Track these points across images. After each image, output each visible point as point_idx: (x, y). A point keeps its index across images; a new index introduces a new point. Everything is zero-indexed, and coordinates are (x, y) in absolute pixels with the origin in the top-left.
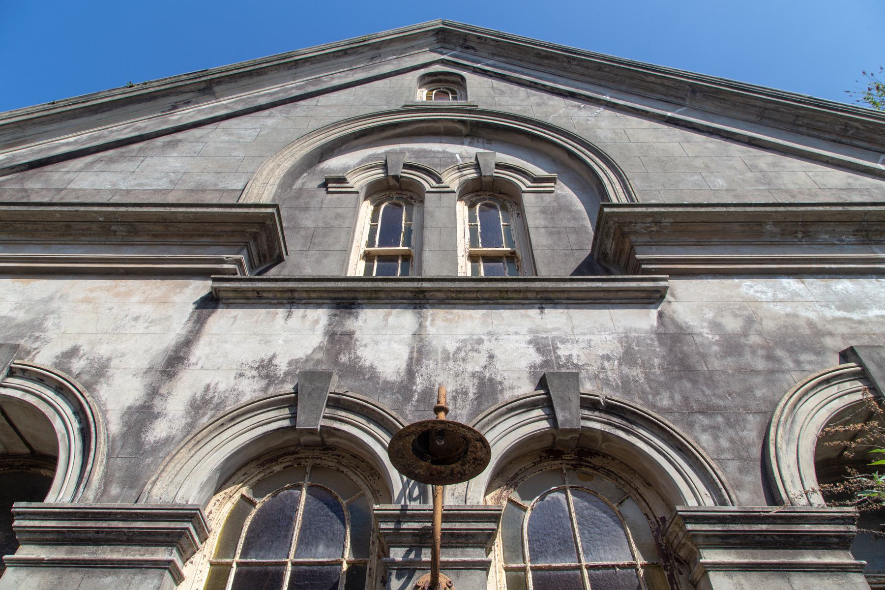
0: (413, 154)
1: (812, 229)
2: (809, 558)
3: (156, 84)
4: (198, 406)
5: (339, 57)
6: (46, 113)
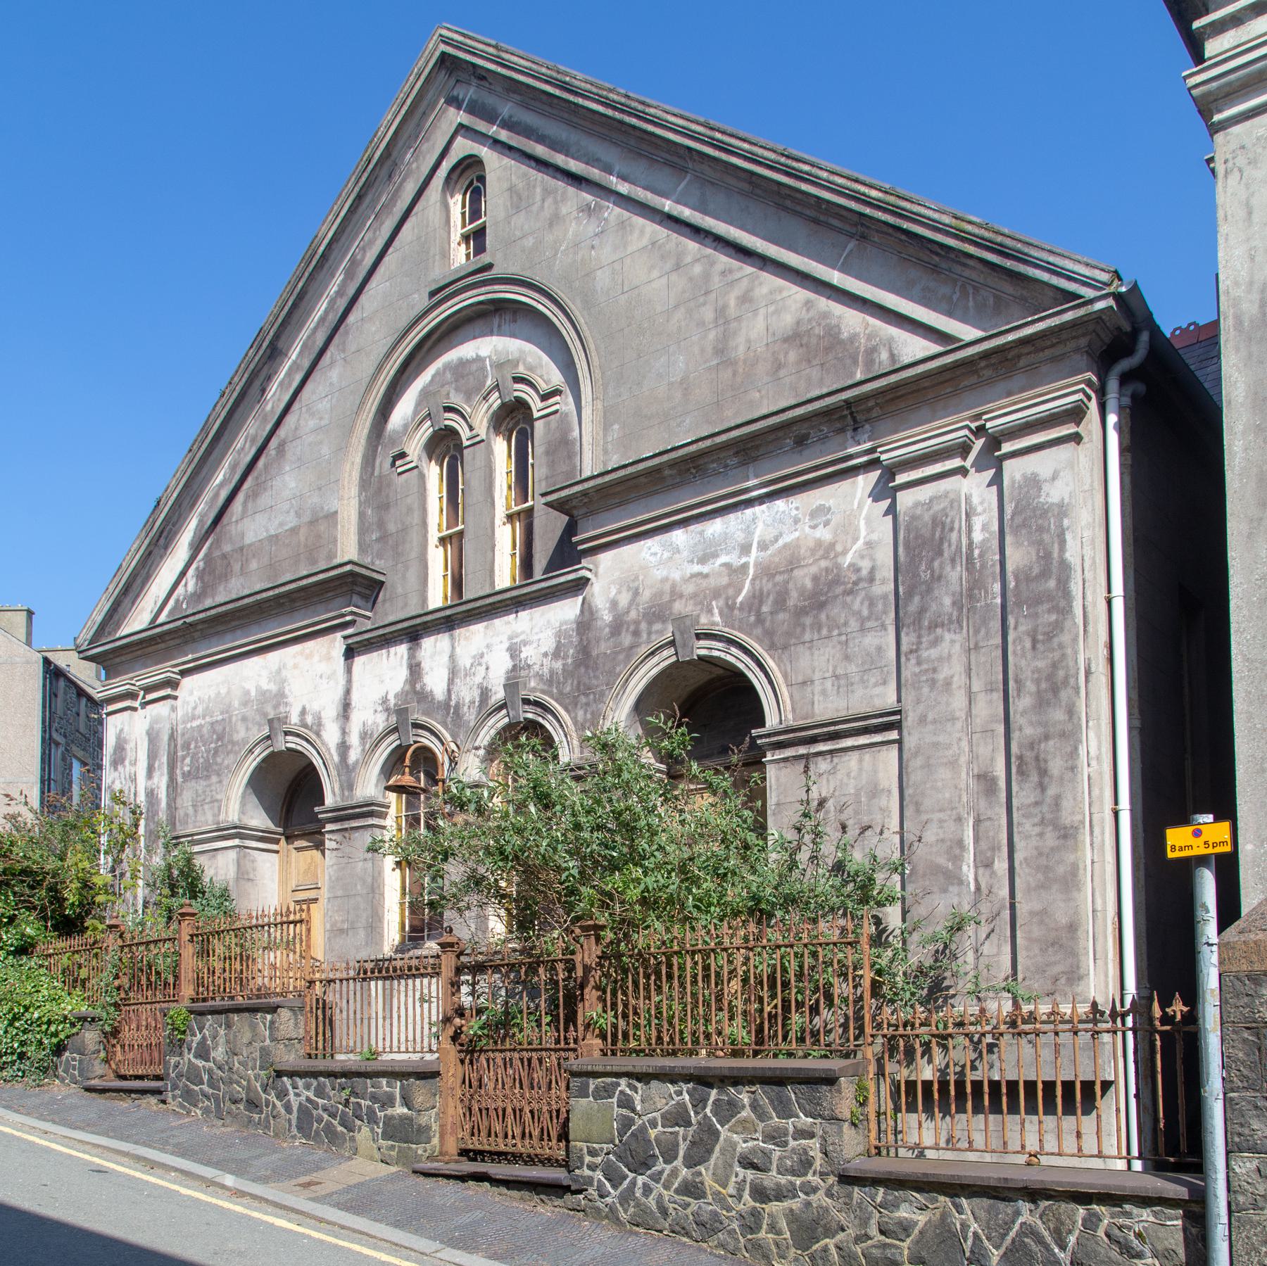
1: (701, 462)
2: (849, 742)
4: (364, 736)
5: (357, 207)
6: (193, 466)
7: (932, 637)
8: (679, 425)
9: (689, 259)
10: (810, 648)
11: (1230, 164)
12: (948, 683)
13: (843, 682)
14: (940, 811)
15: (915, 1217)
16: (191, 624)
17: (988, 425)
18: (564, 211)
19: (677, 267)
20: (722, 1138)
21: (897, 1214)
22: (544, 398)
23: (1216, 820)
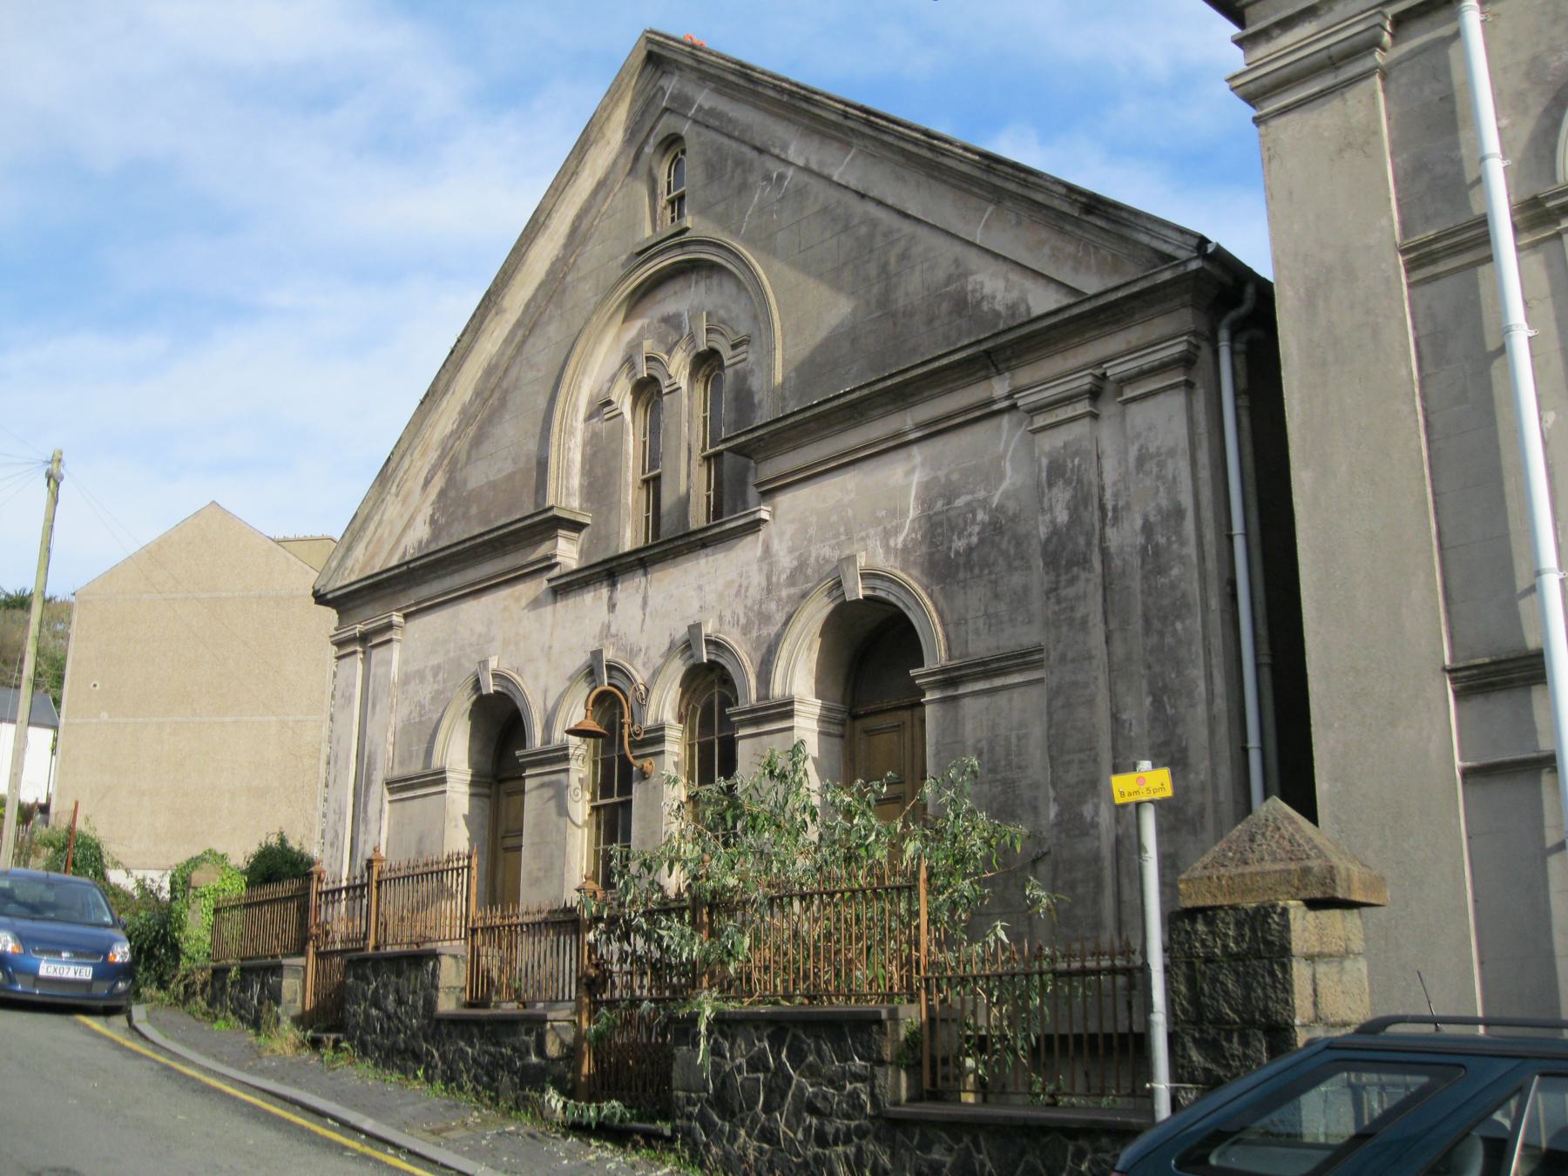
7: (1069, 576)
8: (847, 373)
9: (856, 221)
10: (964, 587)
11: (1272, 152)
12: (1084, 621)
13: (993, 621)
14: (1081, 751)
15: (943, 1159)
16: (414, 569)
17: (1020, 403)
18: (751, 179)
19: (846, 228)
20: (794, 1082)
21: (929, 1157)
22: (734, 347)
23: (1154, 766)
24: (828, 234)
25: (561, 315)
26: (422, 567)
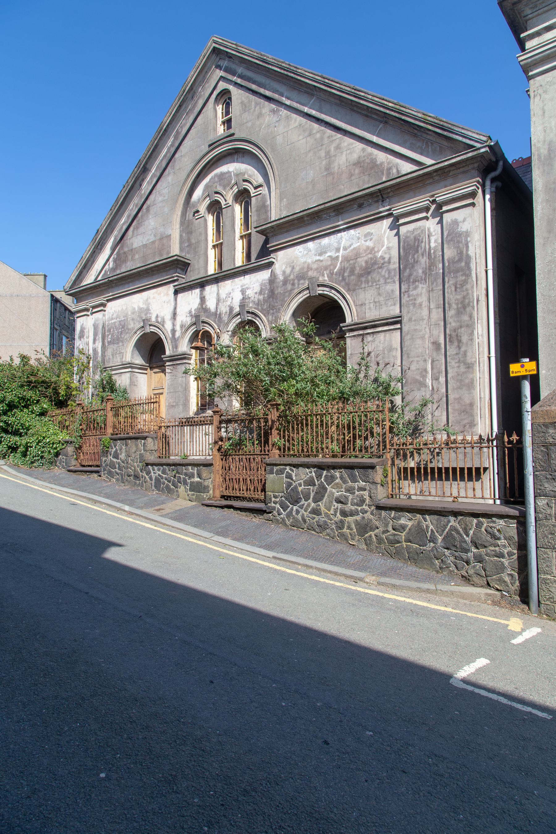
0: (107, 382)
3: (130, 180)
9: (315, 131)
10: (364, 290)
11: (536, 93)
12: (420, 305)
13: (377, 304)
14: (417, 357)
16: (111, 281)
17: (437, 199)
19: (310, 135)
20: (328, 491)
21: (400, 522)
23: (530, 361)
24: (301, 137)
25: (174, 172)
26: (116, 279)
